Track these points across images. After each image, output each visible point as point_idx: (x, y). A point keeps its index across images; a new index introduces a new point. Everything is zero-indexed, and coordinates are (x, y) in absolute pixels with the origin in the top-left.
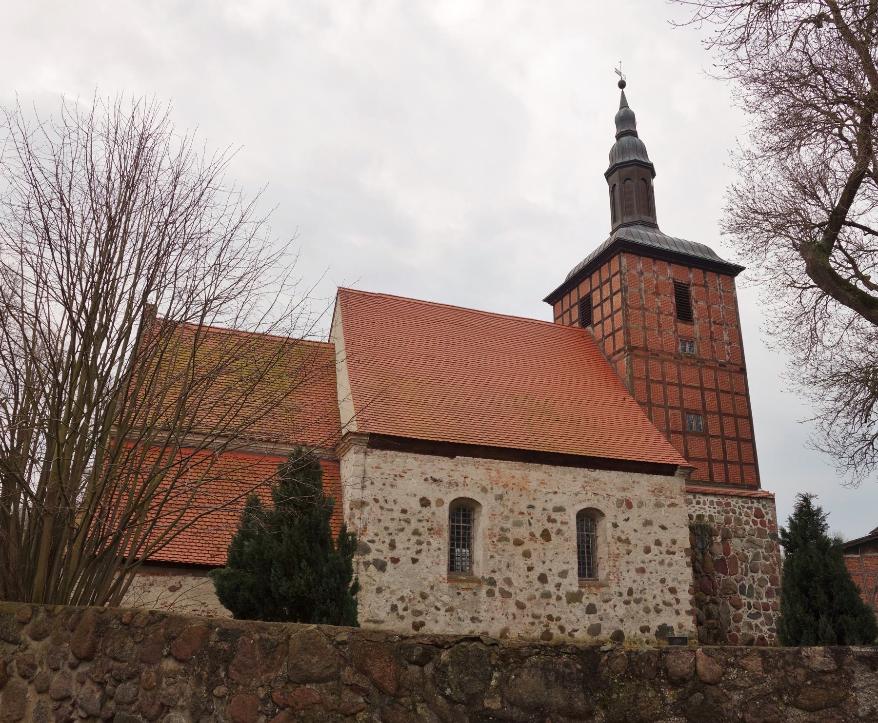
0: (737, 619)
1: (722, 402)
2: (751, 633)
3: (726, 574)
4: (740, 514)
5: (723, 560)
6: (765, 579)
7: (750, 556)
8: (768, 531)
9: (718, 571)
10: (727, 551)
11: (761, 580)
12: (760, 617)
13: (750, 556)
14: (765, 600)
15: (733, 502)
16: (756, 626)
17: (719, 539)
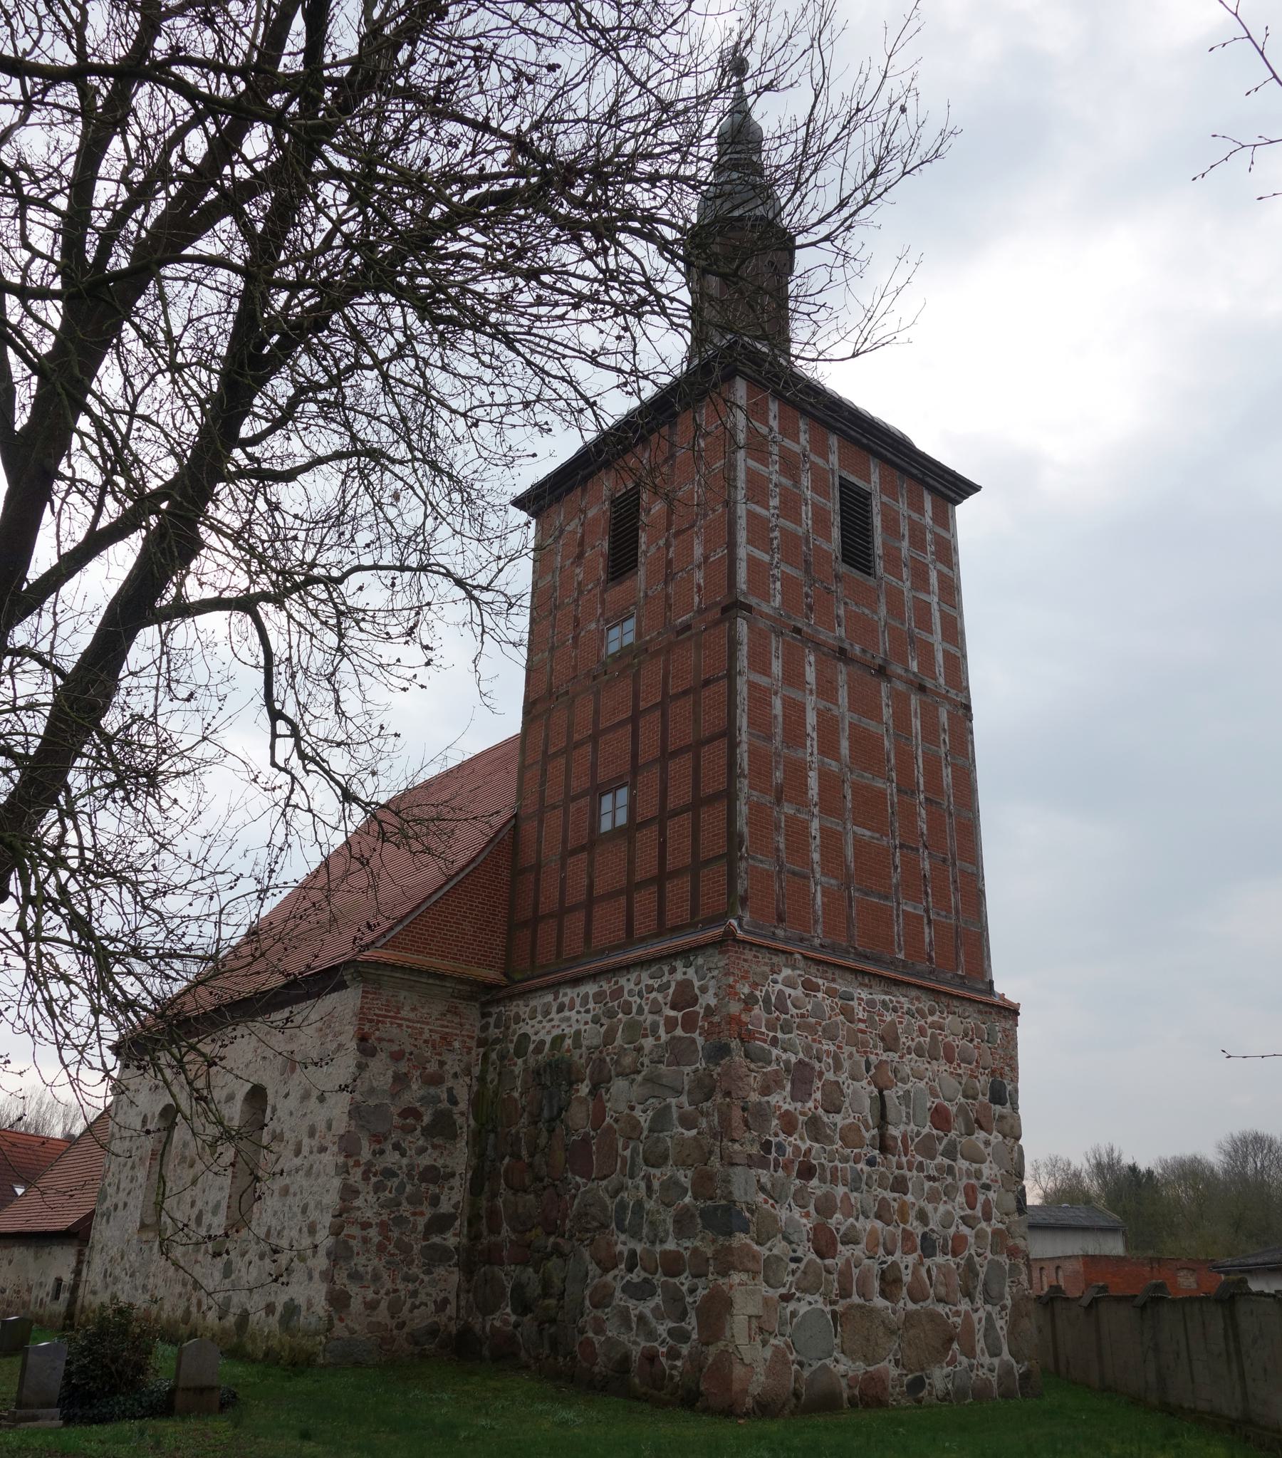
0: (602, 1299)
1: (641, 746)
2: (624, 1338)
3: (589, 1178)
4: (640, 1010)
5: (586, 1140)
6: (677, 1183)
7: (644, 1119)
8: (700, 1041)
9: (574, 1173)
10: (598, 1116)
11: (672, 1184)
12: (653, 1294)
13: (644, 1119)
14: (671, 1245)
15: (627, 983)
16: (641, 1318)
17: (584, 1089)
